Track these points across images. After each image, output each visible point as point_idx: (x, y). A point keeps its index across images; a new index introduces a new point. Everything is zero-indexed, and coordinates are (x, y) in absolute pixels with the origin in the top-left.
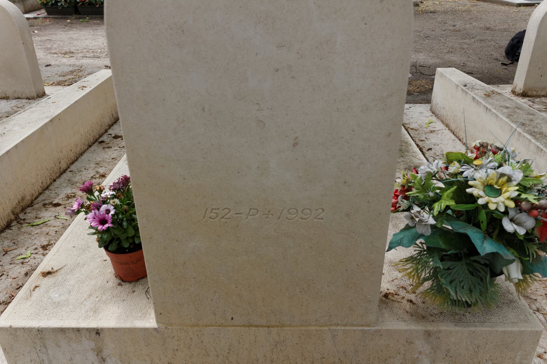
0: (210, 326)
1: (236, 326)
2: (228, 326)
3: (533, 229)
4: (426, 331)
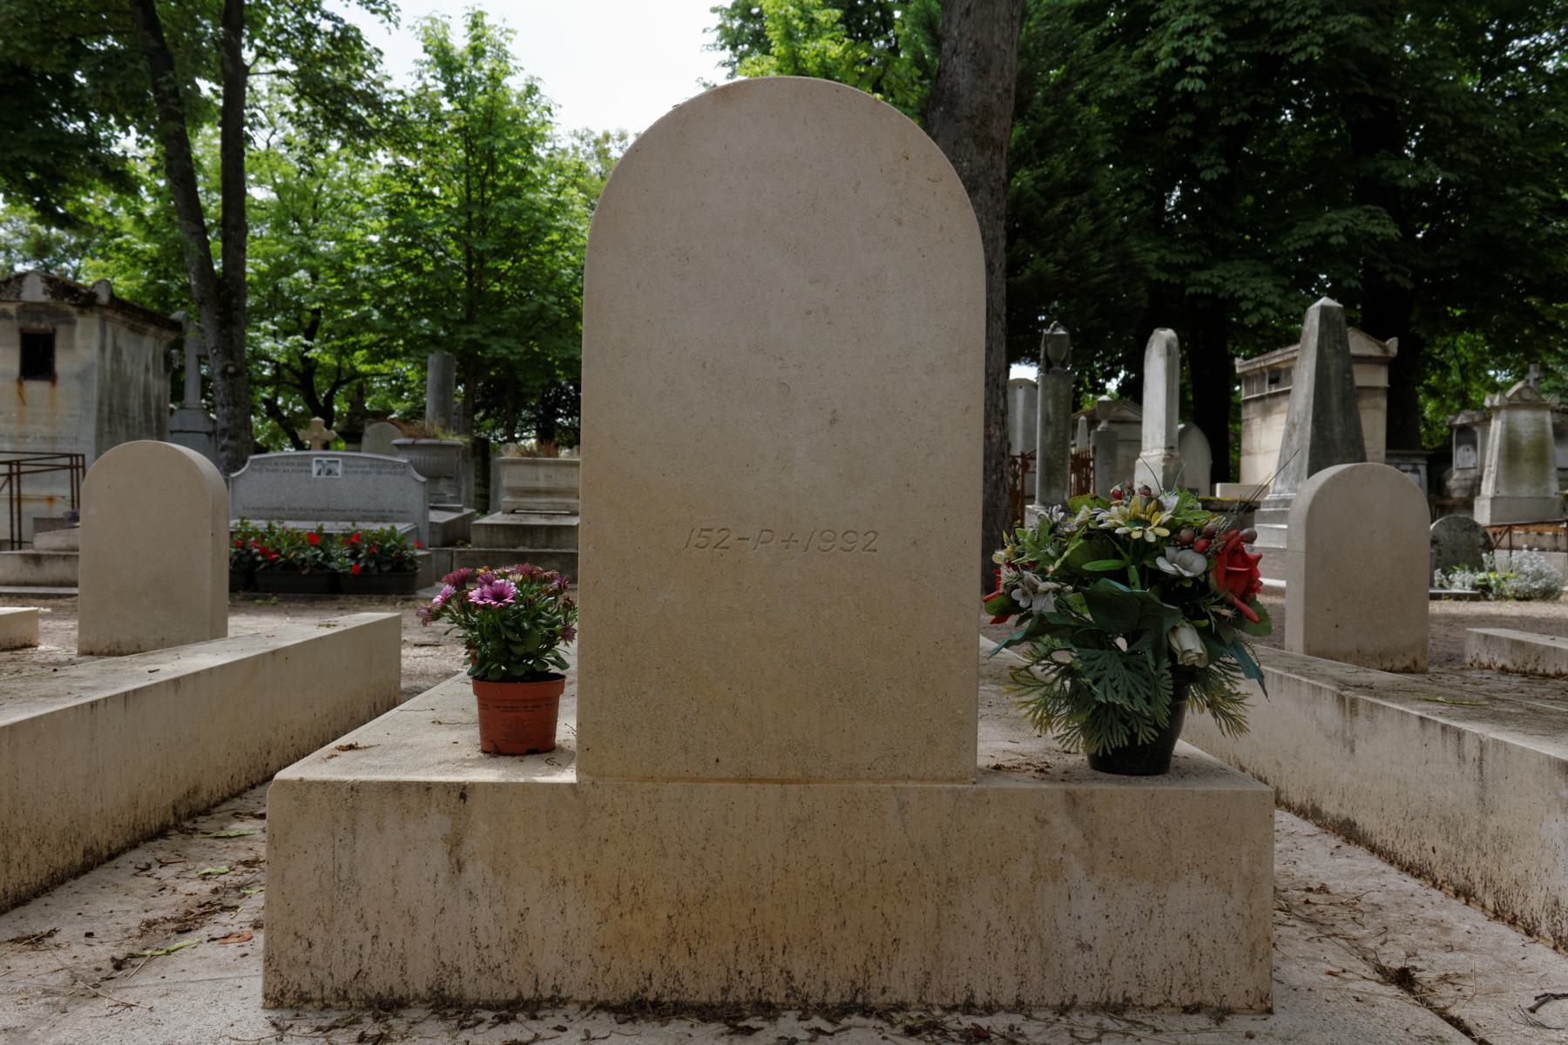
0: (675, 780)
1: (723, 780)
2: (710, 780)
3: (1206, 573)
4: (1068, 793)
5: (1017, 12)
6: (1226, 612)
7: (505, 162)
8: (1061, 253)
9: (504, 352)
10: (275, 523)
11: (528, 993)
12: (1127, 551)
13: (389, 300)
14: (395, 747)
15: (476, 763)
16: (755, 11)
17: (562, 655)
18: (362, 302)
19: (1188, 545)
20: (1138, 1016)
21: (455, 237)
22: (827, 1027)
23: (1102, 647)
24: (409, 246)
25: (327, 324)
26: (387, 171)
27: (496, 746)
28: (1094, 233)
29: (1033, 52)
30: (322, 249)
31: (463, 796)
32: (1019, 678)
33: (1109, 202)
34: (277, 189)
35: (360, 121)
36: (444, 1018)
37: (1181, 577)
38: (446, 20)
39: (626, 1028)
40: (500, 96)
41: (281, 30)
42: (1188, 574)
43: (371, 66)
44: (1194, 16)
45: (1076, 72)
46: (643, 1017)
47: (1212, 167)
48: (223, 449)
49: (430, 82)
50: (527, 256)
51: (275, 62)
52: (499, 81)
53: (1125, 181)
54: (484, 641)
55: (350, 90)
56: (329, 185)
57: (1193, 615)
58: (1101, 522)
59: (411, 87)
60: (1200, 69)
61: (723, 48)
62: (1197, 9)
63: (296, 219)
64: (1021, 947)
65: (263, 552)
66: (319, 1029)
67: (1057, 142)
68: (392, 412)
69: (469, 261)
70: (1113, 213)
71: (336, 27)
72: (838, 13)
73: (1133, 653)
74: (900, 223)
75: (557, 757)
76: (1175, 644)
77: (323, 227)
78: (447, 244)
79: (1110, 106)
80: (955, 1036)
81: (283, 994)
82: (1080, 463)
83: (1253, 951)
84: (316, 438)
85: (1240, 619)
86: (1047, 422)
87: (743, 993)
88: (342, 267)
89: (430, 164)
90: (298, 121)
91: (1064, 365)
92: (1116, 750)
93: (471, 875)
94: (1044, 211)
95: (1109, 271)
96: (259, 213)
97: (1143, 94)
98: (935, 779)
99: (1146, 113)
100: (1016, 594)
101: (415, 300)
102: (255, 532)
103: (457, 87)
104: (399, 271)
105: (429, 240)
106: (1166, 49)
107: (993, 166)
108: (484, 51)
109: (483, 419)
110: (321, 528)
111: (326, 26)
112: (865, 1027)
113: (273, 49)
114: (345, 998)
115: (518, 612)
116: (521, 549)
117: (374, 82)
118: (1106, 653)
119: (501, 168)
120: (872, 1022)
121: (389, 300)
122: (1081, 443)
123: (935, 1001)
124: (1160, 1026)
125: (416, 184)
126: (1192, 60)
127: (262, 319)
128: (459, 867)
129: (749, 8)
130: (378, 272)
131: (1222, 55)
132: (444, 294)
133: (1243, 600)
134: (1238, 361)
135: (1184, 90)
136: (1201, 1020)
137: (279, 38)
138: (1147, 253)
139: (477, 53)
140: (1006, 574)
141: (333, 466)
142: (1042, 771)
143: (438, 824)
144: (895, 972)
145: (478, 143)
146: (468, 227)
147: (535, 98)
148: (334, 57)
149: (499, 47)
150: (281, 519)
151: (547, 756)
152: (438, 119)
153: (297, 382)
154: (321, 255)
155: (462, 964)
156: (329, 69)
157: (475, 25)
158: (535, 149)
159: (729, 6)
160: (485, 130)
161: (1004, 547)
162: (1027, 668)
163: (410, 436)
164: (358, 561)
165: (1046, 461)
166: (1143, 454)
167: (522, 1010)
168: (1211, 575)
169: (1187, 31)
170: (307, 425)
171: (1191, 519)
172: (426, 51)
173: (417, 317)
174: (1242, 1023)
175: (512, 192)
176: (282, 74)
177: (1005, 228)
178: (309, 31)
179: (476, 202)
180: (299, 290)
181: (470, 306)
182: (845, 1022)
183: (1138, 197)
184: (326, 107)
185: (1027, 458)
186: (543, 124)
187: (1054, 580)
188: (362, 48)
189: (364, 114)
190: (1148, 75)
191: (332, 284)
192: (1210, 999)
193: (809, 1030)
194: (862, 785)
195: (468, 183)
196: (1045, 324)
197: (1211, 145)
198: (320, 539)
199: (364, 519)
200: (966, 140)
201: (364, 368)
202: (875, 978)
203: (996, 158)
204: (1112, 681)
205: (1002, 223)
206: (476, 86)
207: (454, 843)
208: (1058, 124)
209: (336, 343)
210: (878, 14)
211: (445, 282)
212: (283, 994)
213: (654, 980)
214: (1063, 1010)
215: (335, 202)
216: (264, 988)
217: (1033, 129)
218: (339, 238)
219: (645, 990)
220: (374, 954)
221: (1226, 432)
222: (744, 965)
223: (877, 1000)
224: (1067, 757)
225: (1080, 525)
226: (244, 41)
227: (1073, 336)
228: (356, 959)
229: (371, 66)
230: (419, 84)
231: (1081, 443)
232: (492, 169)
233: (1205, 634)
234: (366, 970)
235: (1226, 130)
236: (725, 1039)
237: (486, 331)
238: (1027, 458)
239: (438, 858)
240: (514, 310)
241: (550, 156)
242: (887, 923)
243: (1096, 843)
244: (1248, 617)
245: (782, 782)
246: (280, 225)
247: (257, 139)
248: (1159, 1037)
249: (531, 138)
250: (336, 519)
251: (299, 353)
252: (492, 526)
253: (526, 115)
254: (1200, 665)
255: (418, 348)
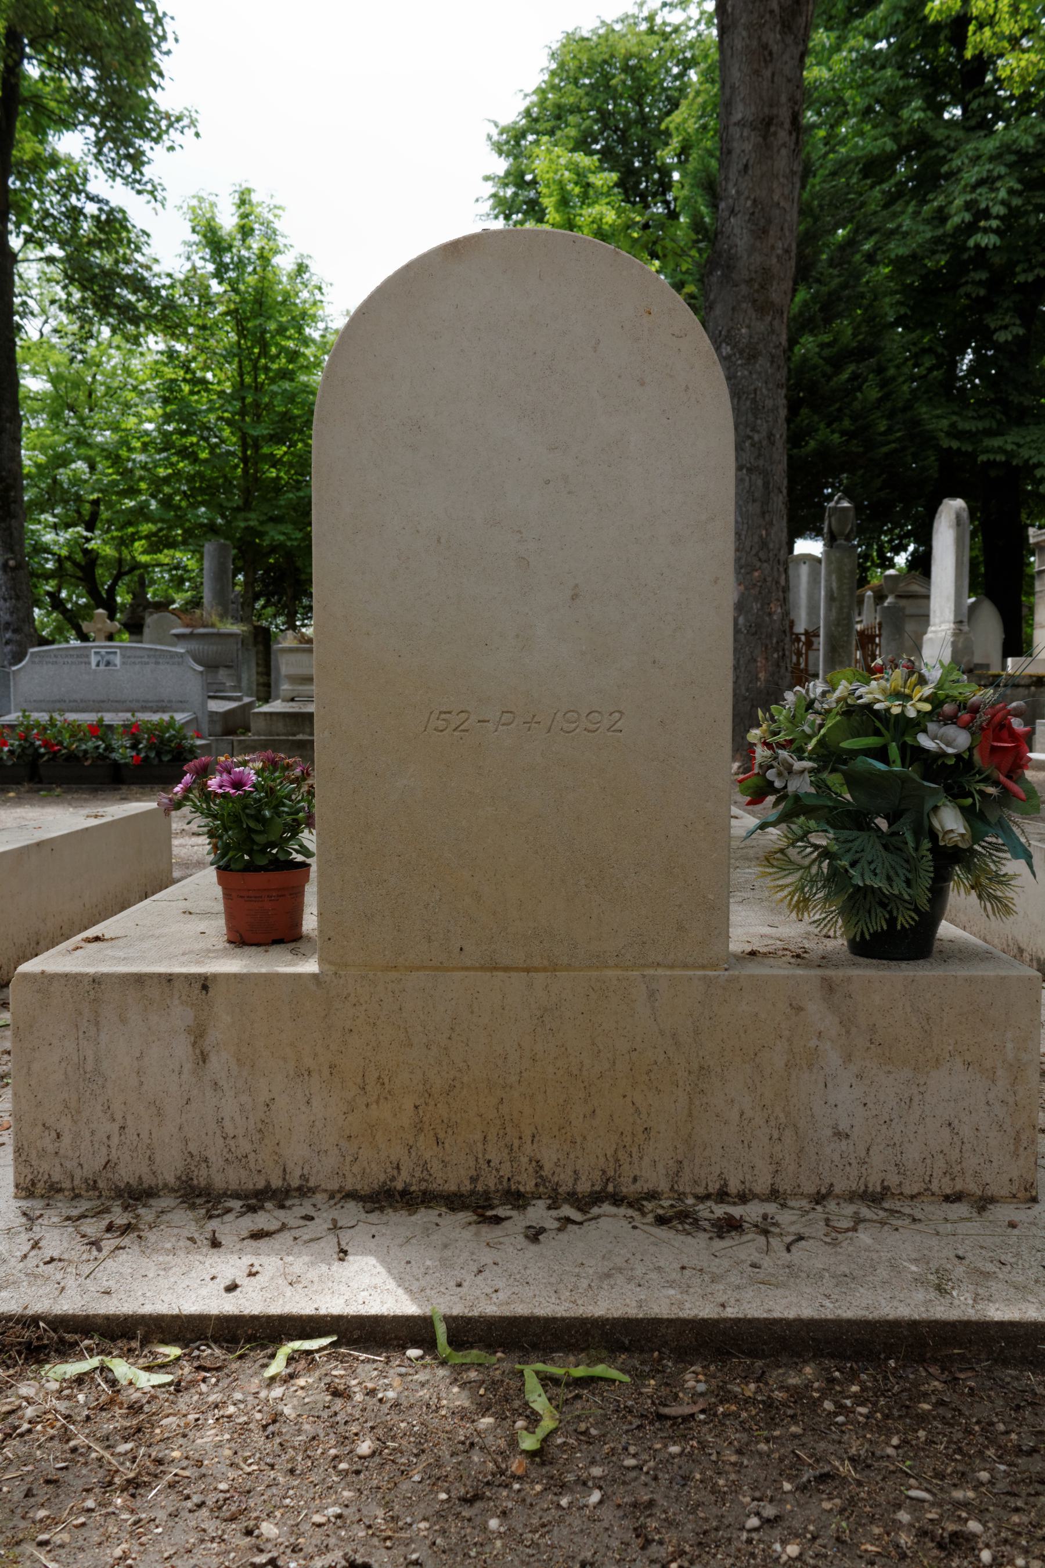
0: (418, 969)
1: (467, 969)
3: (970, 749)
4: (824, 979)
5: (798, 168)
6: (991, 790)
7: (277, 344)
8: (847, 423)
9: (282, 538)
10: (56, 716)
11: (276, 1183)
12: (888, 729)
13: (167, 490)
14: (142, 939)
15: (223, 954)
16: (529, 177)
17: (306, 843)
18: (139, 492)
19: (951, 719)
20: (896, 1205)
21: (229, 422)
22: (577, 1216)
23: (860, 828)
24: (184, 434)
25: (105, 514)
26: (159, 357)
27: (242, 937)
28: (880, 400)
29: (817, 211)
30: (99, 439)
31: (205, 988)
32: (776, 860)
33: (898, 367)
34: (55, 380)
35: (129, 306)
36: (193, 1207)
37: (944, 755)
38: (213, 198)
39: (374, 1217)
40: (270, 276)
41: (47, 214)
42: (950, 751)
43: (138, 249)
44: (988, 166)
45: (863, 230)
46: (391, 1206)
47: (1006, 327)
48: (7, 643)
49: (200, 264)
50: (302, 440)
51: (42, 248)
52: (269, 260)
53: (914, 344)
54: (226, 830)
55: (118, 274)
56: (103, 374)
57: (956, 793)
58: (860, 697)
59: (180, 268)
60: (994, 223)
61: (496, 217)
62: (991, 159)
63: (71, 409)
64: (776, 1136)
65: (46, 744)
66: (68, 1218)
67: (842, 306)
68: (173, 602)
69: (244, 446)
70: (901, 379)
71: (101, 210)
72: (614, 176)
73: (894, 834)
74: (643, 384)
75: (302, 946)
76: (936, 824)
77: (98, 416)
78: (221, 430)
79: (901, 265)
80: (706, 1224)
81: (33, 1184)
82: (866, 640)
83: (1017, 1139)
84: (100, 630)
85: (1006, 798)
86: (831, 598)
87: (492, 1183)
88: (118, 456)
89: (202, 350)
90: (69, 309)
91: (848, 539)
92: (874, 935)
93: (216, 1064)
94: (829, 379)
95: (898, 440)
96: (37, 405)
97: (934, 252)
98: (686, 966)
99: (937, 272)
100: (771, 774)
101: (191, 489)
102: (37, 725)
103: (227, 269)
104: (174, 459)
105: (205, 427)
106: (959, 202)
107: (773, 332)
108: (252, 230)
109: (264, 607)
110: (101, 720)
111: (91, 208)
112: (615, 1216)
113: (40, 234)
114: (95, 1187)
115: (260, 800)
116: (300, 737)
117: (141, 266)
118: (864, 835)
119: (274, 350)
120: (622, 1211)
121: (167, 490)
122: (866, 620)
123: (688, 1190)
124: (918, 1215)
125: (188, 370)
126: (986, 214)
127: (42, 512)
128: (204, 1058)
129: (522, 175)
130: (154, 461)
131: (1018, 208)
132: (221, 481)
133: (1010, 778)
134: (1031, 531)
135: (977, 246)
136: (961, 1209)
137: (46, 223)
138: (937, 420)
139: (246, 232)
140: (761, 753)
141: (111, 657)
142: (798, 956)
143: (181, 1015)
144: (646, 1160)
145: (250, 325)
146: (243, 413)
147: (306, 276)
148: (101, 241)
149: (268, 224)
150: (62, 711)
151: (293, 945)
152: (208, 302)
153: (80, 574)
154: (97, 445)
155: (210, 1154)
156: (97, 253)
157: (243, 202)
158: (307, 331)
159: (502, 174)
160: (259, 314)
161: (759, 726)
162: (782, 851)
163: (187, 626)
164: (139, 751)
165: (831, 638)
166: (931, 629)
167: (270, 1199)
168: (976, 752)
169: (980, 183)
170: (90, 617)
171: (955, 693)
172: (194, 231)
173: (195, 506)
174: (1003, 1212)
175: (286, 375)
176: (50, 260)
177: (786, 397)
178: (75, 214)
179: (250, 387)
180: (76, 481)
181: (247, 493)
182: (595, 1211)
183: (928, 361)
184: (94, 293)
185: (811, 635)
186: (315, 303)
187: (810, 759)
188: (128, 231)
189: (132, 298)
190: (940, 232)
191: (108, 474)
192: (972, 1187)
193: (559, 1219)
194: (610, 973)
195: (240, 367)
196: (830, 498)
197: (1006, 304)
198: (100, 730)
199: (144, 709)
200: (744, 305)
201: (144, 558)
202: (626, 1167)
203: (776, 323)
204: (870, 863)
205: (783, 392)
206: (245, 266)
207: (198, 1034)
208: (844, 286)
209: (115, 534)
210: (656, 176)
211: (221, 470)
212: (33, 1184)
213: (403, 1168)
214: (819, 1199)
215: (110, 392)
216: (15, 1178)
217: (817, 292)
218: (115, 428)
219: (393, 1179)
220: (121, 1144)
221: (1020, 604)
222: (493, 1155)
223: (628, 1189)
224: (826, 941)
225: (838, 701)
226: (11, 227)
227: (858, 508)
228: (104, 1150)
229: (138, 249)
230: (188, 266)
231: (866, 620)
232: (264, 352)
233: (969, 814)
234: (115, 1160)
235: (1022, 287)
236: (473, 1228)
237: (263, 518)
238: (811, 635)
239: (182, 1049)
240: (291, 495)
241: (323, 336)
242: (638, 1111)
243: (854, 1030)
244: (1015, 795)
245: (528, 970)
246: (55, 415)
247: (28, 328)
248: (918, 1226)
249: (302, 318)
250: (116, 711)
251: (75, 544)
252: (271, 714)
253: (297, 294)
254: (964, 846)
255: (196, 536)
